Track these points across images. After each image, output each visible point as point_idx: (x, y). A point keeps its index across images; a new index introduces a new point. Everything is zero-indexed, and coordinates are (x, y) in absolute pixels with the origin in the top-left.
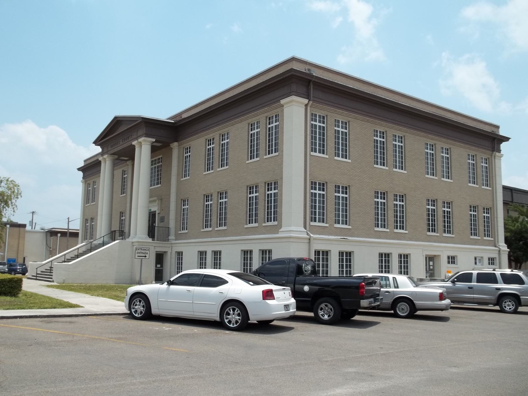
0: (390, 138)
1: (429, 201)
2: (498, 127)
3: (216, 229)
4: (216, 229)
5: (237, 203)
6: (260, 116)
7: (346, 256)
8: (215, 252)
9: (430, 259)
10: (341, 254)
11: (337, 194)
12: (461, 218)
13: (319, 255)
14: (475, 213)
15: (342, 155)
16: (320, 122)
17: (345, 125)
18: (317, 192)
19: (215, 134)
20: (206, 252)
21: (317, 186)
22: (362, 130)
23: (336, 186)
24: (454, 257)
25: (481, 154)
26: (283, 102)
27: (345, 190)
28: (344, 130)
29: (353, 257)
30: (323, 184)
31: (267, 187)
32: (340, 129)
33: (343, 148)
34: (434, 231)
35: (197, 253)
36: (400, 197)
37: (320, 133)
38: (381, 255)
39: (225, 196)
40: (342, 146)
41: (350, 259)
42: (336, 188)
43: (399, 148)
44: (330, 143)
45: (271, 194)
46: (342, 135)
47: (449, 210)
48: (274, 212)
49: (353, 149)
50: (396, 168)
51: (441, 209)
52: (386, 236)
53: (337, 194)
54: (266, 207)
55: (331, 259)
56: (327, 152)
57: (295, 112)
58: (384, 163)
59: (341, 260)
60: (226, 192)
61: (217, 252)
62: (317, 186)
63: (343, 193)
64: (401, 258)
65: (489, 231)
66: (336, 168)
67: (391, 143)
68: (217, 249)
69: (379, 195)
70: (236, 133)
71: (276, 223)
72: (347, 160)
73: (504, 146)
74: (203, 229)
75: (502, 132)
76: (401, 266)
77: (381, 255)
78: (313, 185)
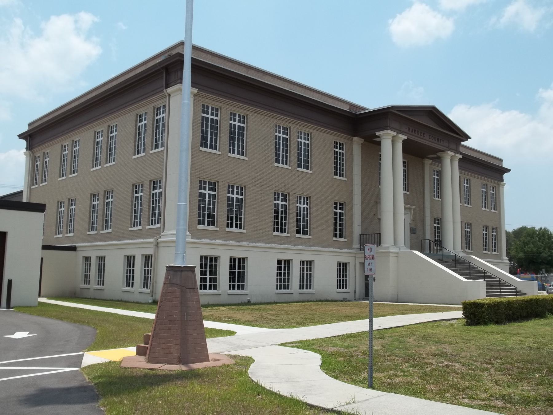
0: (294, 135)
1: (336, 204)
2: (501, 160)
3: (102, 232)
4: (102, 232)
5: (121, 201)
6: (146, 108)
7: (285, 264)
8: (128, 257)
9: (283, 266)
10: (233, 260)
11: (276, 202)
12: (321, 217)
13: (235, 262)
14: (341, 211)
15: (283, 161)
16: (239, 122)
17: (242, 119)
18: (235, 196)
19: (101, 127)
20: (134, 257)
21: (235, 190)
22: (261, 126)
23: (275, 193)
24: (346, 264)
25: (491, 183)
26: (355, 138)
27: (307, 200)
28: (285, 136)
29: (314, 265)
30: (242, 189)
31: (152, 186)
32: (281, 135)
33: (304, 160)
34: (283, 230)
35: (123, 256)
36: (340, 205)
37: (239, 133)
38: (279, 262)
39: (112, 196)
40: (283, 152)
41: (289, 268)
42: (275, 195)
43: (340, 155)
44: (293, 156)
45: (156, 193)
46: (283, 140)
47: (438, 225)
48: (156, 215)
49: (250, 143)
50: (301, 167)
51: (292, 207)
52: (287, 241)
53: (276, 202)
54: (148, 208)
55: (220, 266)
56: (246, 154)
57: (182, 101)
58: (308, 166)
59: (302, 269)
60: (112, 191)
61: (131, 257)
62: (235, 190)
63: (282, 201)
64: (340, 266)
65: (496, 248)
66: (224, 164)
67: (294, 140)
68: (101, 254)
69: (338, 206)
70: (123, 124)
71: (158, 226)
72: (287, 167)
73: (506, 176)
74: (103, 230)
75: (505, 165)
76: (340, 274)
77: (279, 262)
78: (202, 184)
